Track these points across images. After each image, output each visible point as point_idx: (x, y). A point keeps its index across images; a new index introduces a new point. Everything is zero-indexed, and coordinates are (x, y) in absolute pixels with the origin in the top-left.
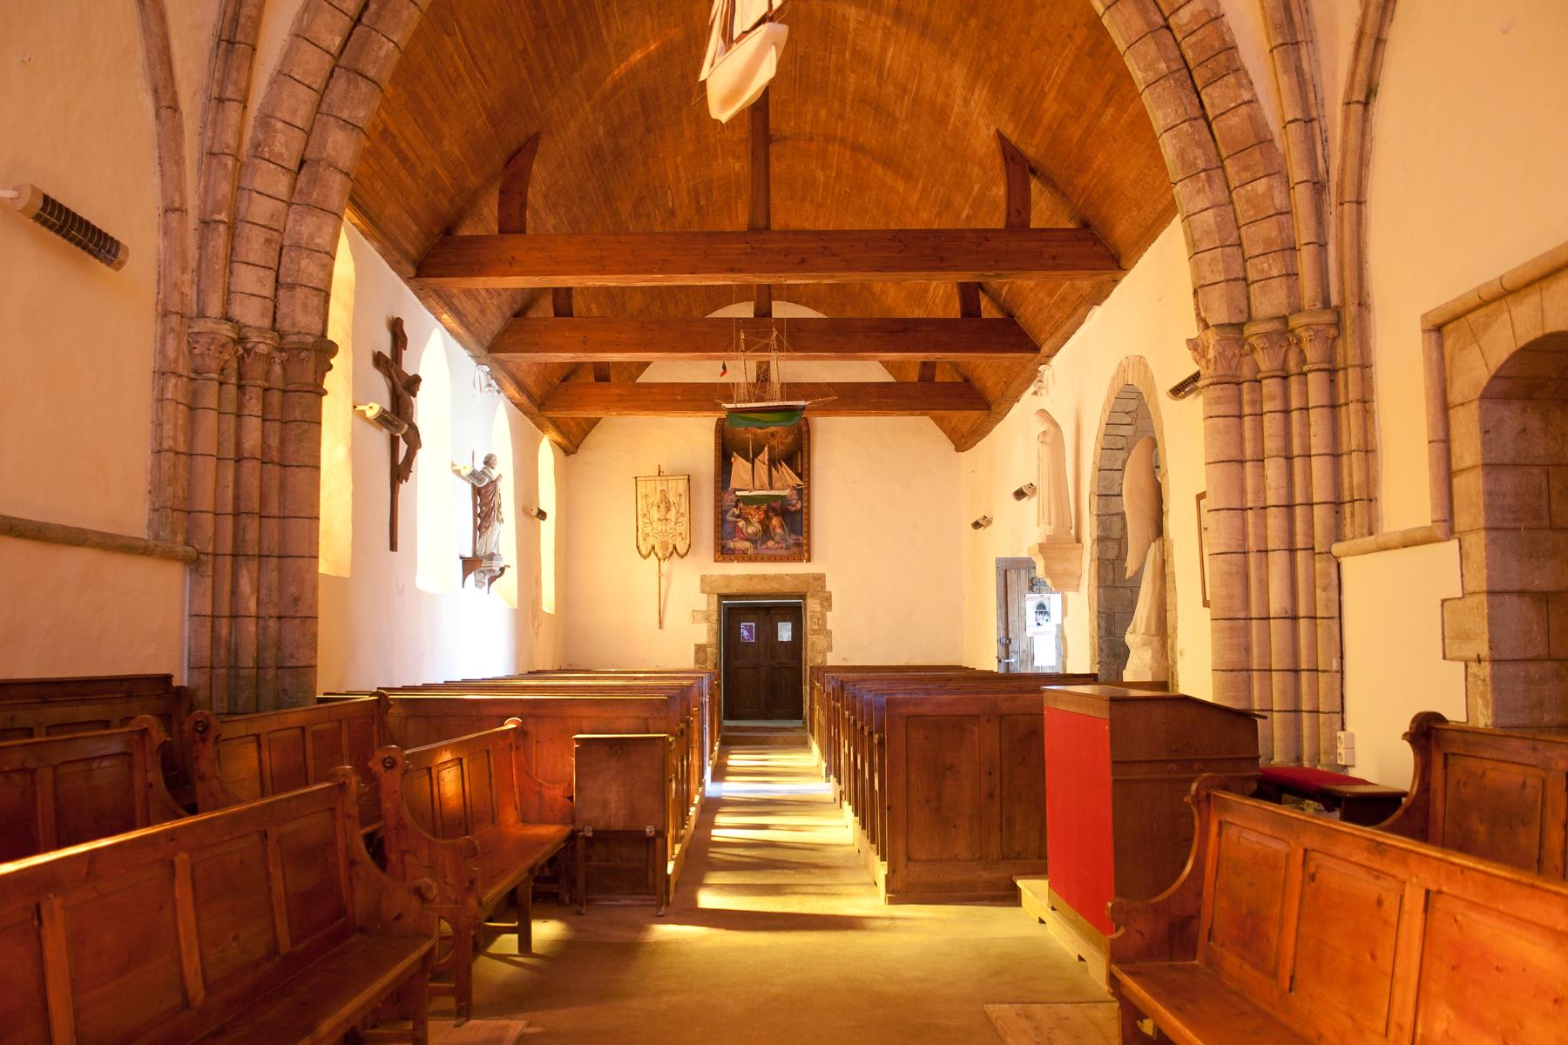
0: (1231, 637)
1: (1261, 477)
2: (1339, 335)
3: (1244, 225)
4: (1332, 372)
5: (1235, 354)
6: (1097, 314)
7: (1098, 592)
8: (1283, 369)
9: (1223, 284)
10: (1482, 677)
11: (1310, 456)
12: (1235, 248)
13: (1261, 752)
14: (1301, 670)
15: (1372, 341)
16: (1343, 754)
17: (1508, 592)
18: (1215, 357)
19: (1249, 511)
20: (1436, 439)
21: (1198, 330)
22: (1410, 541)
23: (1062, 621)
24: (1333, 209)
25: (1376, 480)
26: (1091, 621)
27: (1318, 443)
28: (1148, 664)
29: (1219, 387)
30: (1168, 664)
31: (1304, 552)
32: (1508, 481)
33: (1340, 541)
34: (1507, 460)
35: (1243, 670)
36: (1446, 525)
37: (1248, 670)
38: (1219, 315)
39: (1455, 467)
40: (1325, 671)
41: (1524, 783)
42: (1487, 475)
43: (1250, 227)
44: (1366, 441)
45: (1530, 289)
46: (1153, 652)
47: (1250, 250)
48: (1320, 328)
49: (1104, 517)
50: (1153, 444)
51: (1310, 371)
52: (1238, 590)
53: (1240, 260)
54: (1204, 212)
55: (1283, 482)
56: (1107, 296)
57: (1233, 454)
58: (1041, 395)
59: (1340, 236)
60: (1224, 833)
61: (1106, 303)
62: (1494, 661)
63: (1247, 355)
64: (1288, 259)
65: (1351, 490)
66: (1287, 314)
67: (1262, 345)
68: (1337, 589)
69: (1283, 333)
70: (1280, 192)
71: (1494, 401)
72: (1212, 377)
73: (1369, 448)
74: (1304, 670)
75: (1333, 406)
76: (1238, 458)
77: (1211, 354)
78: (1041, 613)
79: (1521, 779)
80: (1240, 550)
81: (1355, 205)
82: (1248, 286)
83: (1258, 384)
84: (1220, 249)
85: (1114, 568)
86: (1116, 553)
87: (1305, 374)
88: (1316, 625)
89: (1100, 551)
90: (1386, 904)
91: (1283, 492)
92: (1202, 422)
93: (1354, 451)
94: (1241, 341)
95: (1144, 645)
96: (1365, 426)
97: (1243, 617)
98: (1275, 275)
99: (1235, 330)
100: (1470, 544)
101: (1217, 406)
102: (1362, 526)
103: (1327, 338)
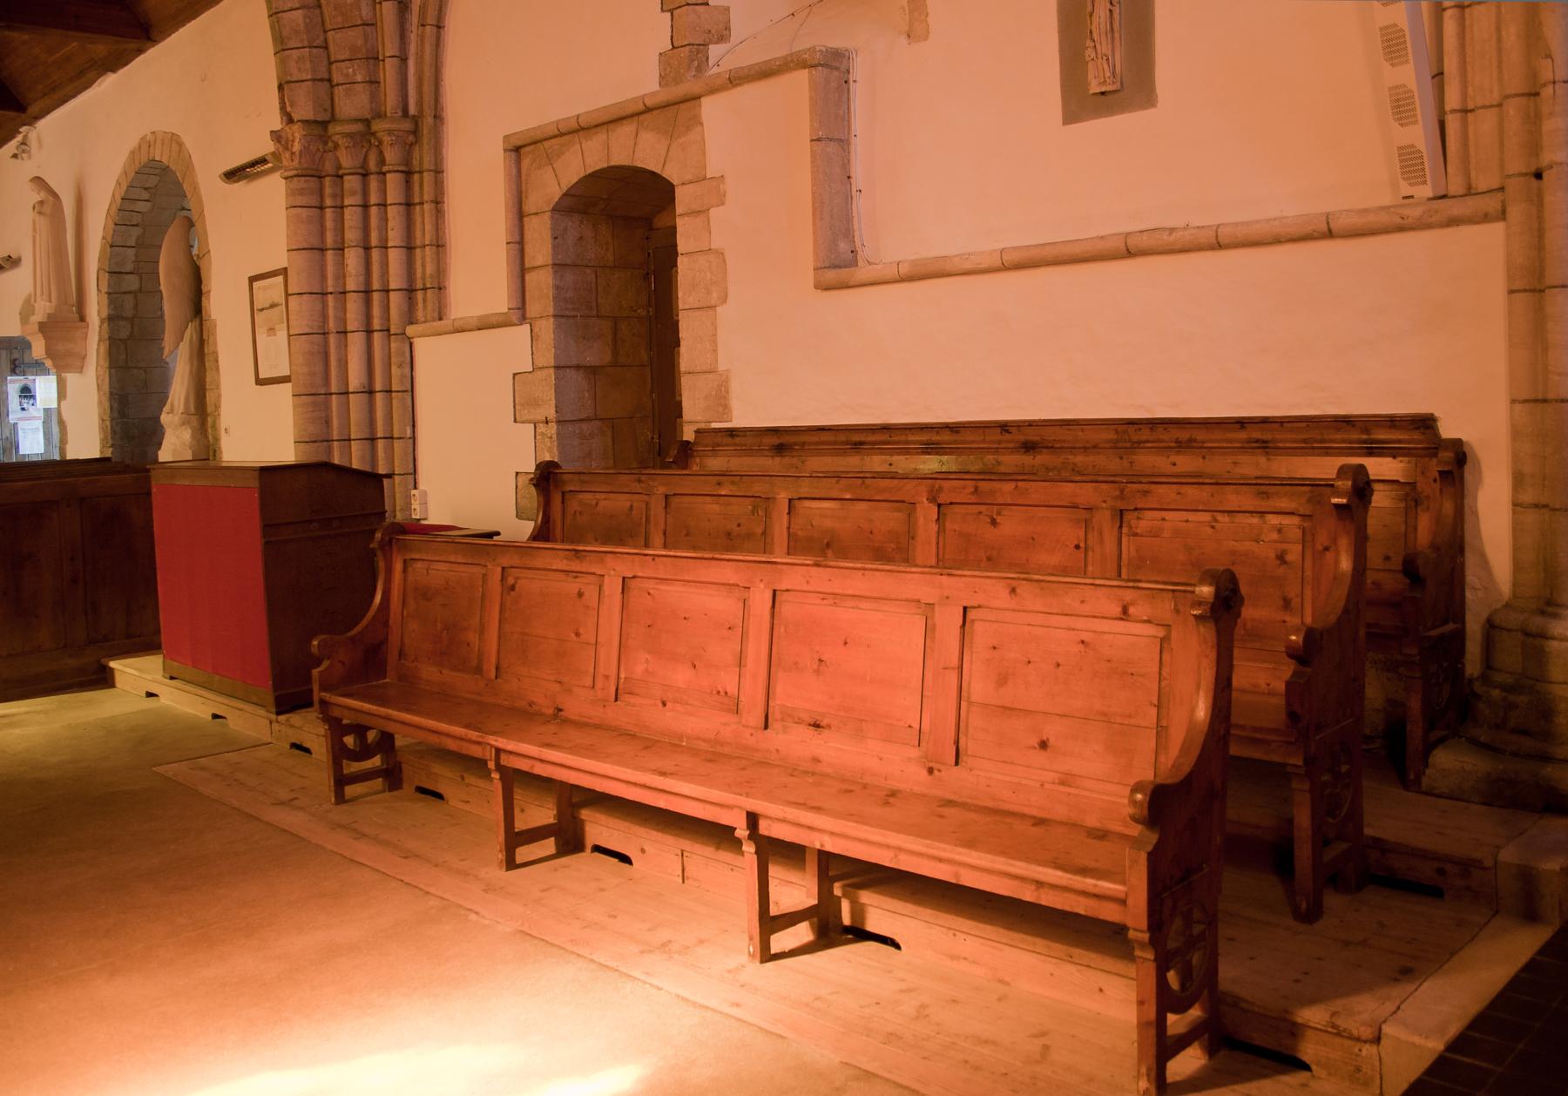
0: (313, 411)
1: (341, 264)
2: (416, 142)
3: (331, 30)
4: (408, 174)
5: (318, 149)
6: (109, 81)
7: (110, 373)
8: (362, 168)
9: (310, 83)
10: (549, 435)
11: (386, 248)
12: (322, 50)
13: (387, 508)
14: (377, 438)
15: (444, 150)
16: (418, 510)
17: (569, 367)
18: (301, 151)
19: (329, 295)
20: (513, 241)
21: (282, 123)
22: (485, 324)
23: (59, 405)
24: (414, 28)
25: (445, 271)
26: (100, 403)
27: (395, 236)
28: (187, 443)
29: (303, 178)
30: (209, 441)
31: (380, 333)
32: (569, 277)
33: (412, 323)
34: (569, 262)
35: (324, 441)
36: (519, 312)
37: (327, 441)
38: (305, 110)
39: (527, 265)
40: (400, 438)
41: (631, 506)
42: (556, 272)
43: (337, 33)
44: (438, 238)
45: (598, 129)
46: (193, 431)
47: (337, 52)
48: (400, 134)
49: (115, 296)
50: (190, 224)
51: (389, 172)
52: (319, 368)
53: (325, 62)
54: (293, 12)
55: (362, 270)
56: (126, 64)
57: (316, 243)
58: (23, 159)
59: (420, 54)
60: (410, 569)
61: (122, 72)
62: (559, 422)
63: (330, 151)
64: (371, 68)
65: (423, 278)
66: (369, 117)
67: (347, 144)
68: (409, 365)
69: (365, 135)
70: (367, 4)
71: (562, 213)
72: (297, 170)
73: (440, 244)
74: (380, 438)
75: (409, 205)
76: (320, 247)
77: (297, 147)
78: (25, 397)
79: (627, 504)
80: (321, 331)
81: (435, 28)
82: (332, 87)
83: (338, 179)
84: (307, 49)
85: (126, 348)
86: (128, 333)
87: (384, 174)
88: (391, 398)
89: (111, 330)
90: (587, 595)
91: (362, 278)
92: (284, 211)
93: (428, 245)
94: (324, 138)
95: (183, 424)
96: (437, 224)
97: (323, 392)
98: (359, 80)
99: (320, 127)
100: (540, 329)
101: (300, 197)
102: (433, 310)
103: (406, 143)
